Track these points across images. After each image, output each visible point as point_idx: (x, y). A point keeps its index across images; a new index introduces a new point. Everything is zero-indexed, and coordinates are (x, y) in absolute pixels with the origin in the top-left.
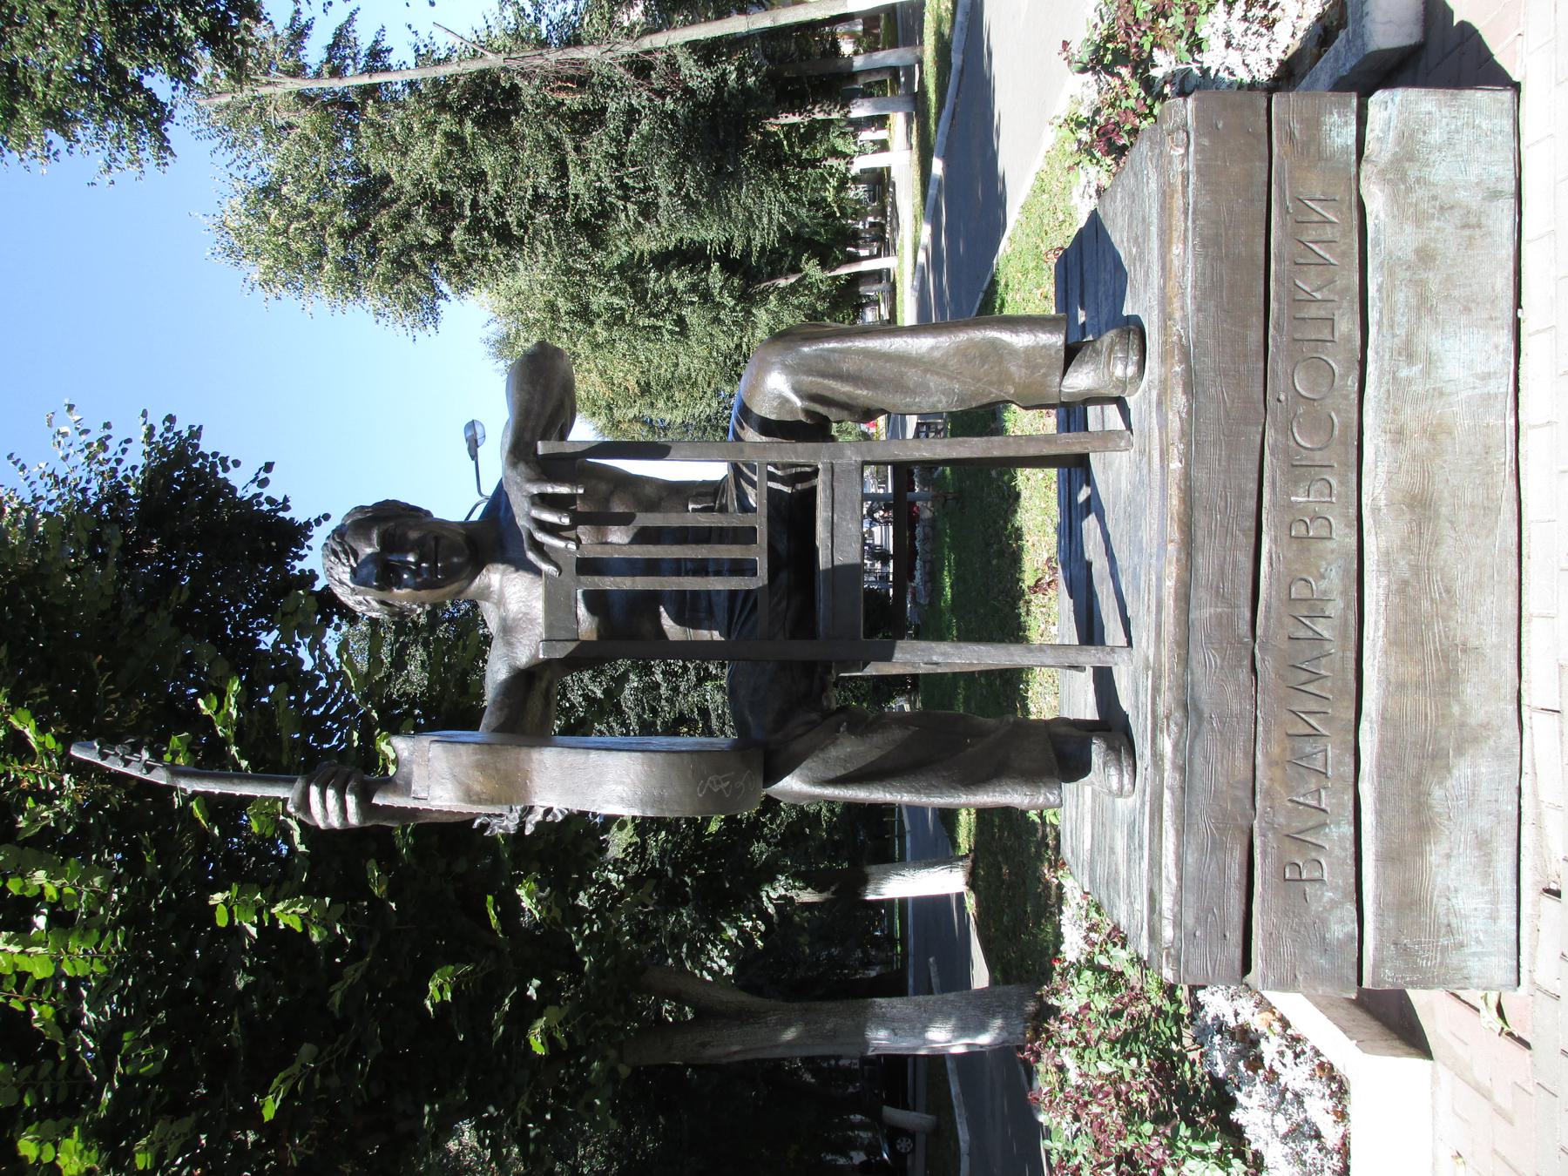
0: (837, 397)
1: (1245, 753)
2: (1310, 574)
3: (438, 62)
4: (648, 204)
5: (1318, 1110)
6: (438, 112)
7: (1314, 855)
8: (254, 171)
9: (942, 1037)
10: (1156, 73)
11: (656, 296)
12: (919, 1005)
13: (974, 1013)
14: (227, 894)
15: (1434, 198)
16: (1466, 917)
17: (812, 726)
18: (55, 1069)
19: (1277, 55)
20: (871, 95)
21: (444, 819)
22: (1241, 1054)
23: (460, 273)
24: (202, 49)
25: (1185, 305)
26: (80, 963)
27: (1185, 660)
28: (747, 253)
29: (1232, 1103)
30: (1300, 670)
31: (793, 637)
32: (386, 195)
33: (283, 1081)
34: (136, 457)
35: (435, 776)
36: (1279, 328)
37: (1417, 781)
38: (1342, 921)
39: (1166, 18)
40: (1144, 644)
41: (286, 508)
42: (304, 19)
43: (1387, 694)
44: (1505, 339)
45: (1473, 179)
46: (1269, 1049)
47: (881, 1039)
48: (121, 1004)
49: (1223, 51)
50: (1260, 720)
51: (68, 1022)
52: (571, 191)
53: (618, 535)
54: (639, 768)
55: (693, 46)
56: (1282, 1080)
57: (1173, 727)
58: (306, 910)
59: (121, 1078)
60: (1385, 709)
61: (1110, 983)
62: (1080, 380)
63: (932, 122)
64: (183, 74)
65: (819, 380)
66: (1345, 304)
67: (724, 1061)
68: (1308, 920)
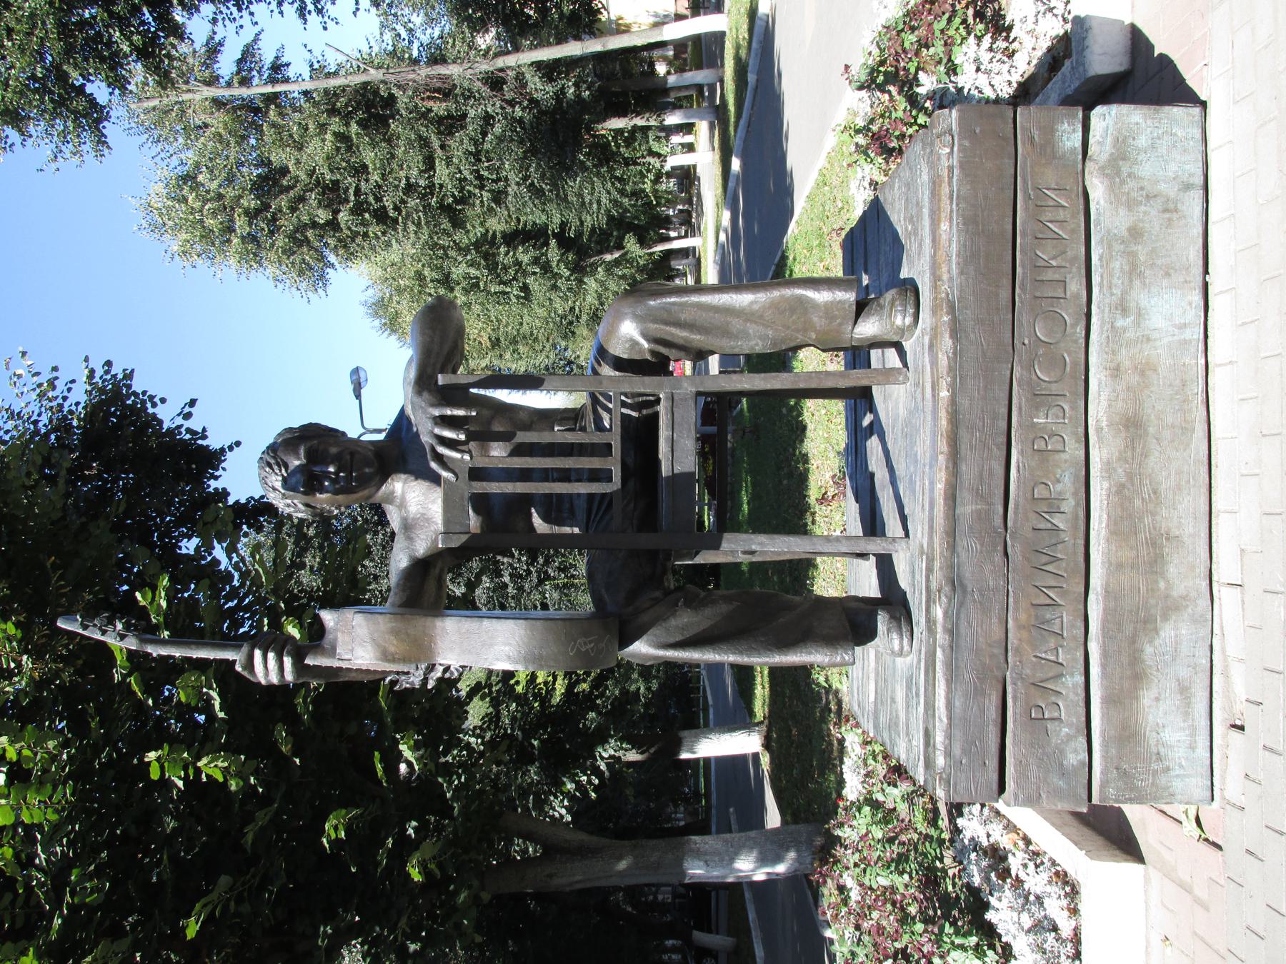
0: (676, 341)
1: (1000, 622)
2: (1048, 479)
3: (328, 75)
4: (499, 192)
5: (1055, 908)
6: (329, 116)
7: (1053, 699)
8: (175, 161)
9: (747, 867)
10: (921, 91)
11: (505, 268)
12: (726, 841)
13: (771, 849)
14: (160, 752)
15: (1142, 189)
16: (1171, 747)
17: (656, 601)
18: (13, 903)
19: (1016, 78)
20: (681, 107)
21: (359, 678)
22: (992, 867)
23: (345, 247)
24: (136, 62)
25: (951, 268)
26: (36, 812)
27: (952, 547)
28: (579, 234)
29: (986, 906)
30: (1042, 553)
31: (640, 530)
32: (285, 183)
33: (205, 906)
34: (79, 395)
35: (357, 643)
36: (1023, 289)
37: (1133, 641)
38: (1075, 751)
39: (928, 47)
40: (919, 535)
41: (204, 437)
42: (217, 38)
43: (1109, 574)
44: (1197, 299)
45: (1171, 174)
46: (1015, 863)
47: (696, 871)
48: (71, 844)
49: (975, 76)
50: (1011, 593)
51: (25, 861)
52: (437, 181)
53: (498, 451)
54: (522, 632)
55: (538, 65)
56: (1026, 886)
57: (943, 598)
58: (226, 764)
59: (69, 906)
60: (1107, 584)
61: (884, 817)
62: (868, 328)
63: (732, 129)
64: (118, 83)
65: (663, 327)
66: (1074, 270)
67: (568, 889)
68: (1049, 750)
